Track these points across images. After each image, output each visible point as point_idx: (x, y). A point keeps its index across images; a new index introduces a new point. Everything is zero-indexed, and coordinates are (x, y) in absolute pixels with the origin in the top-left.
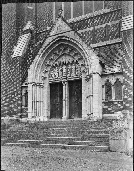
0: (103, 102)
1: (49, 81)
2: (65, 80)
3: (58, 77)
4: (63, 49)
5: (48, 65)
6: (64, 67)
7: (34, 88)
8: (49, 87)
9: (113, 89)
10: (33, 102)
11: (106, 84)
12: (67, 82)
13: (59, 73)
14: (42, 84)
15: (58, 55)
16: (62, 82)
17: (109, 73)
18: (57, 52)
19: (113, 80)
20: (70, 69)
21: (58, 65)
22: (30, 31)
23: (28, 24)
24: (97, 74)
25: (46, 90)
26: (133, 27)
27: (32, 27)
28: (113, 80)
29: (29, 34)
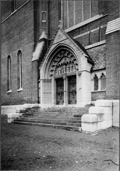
0: (92, 92)
1: (55, 77)
2: (65, 76)
3: (61, 74)
4: (63, 52)
5: (53, 66)
6: (64, 67)
7: (44, 83)
8: (55, 82)
9: (100, 82)
10: (44, 93)
11: (94, 78)
12: (66, 78)
13: (61, 71)
14: (50, 80)
15: (60, 57)
16: (63, 77)
17: (96, 69)
18: (56, 60)
19: (99, 74)
20: (68, 67)
21: (61, 65)
22: (44, 39)
23: (42, 34)
24: (85, 72)
25: (53, 83)
26: (119, 29)
27: (46, 36)
28: (99, 74)
29: (43, 42)
